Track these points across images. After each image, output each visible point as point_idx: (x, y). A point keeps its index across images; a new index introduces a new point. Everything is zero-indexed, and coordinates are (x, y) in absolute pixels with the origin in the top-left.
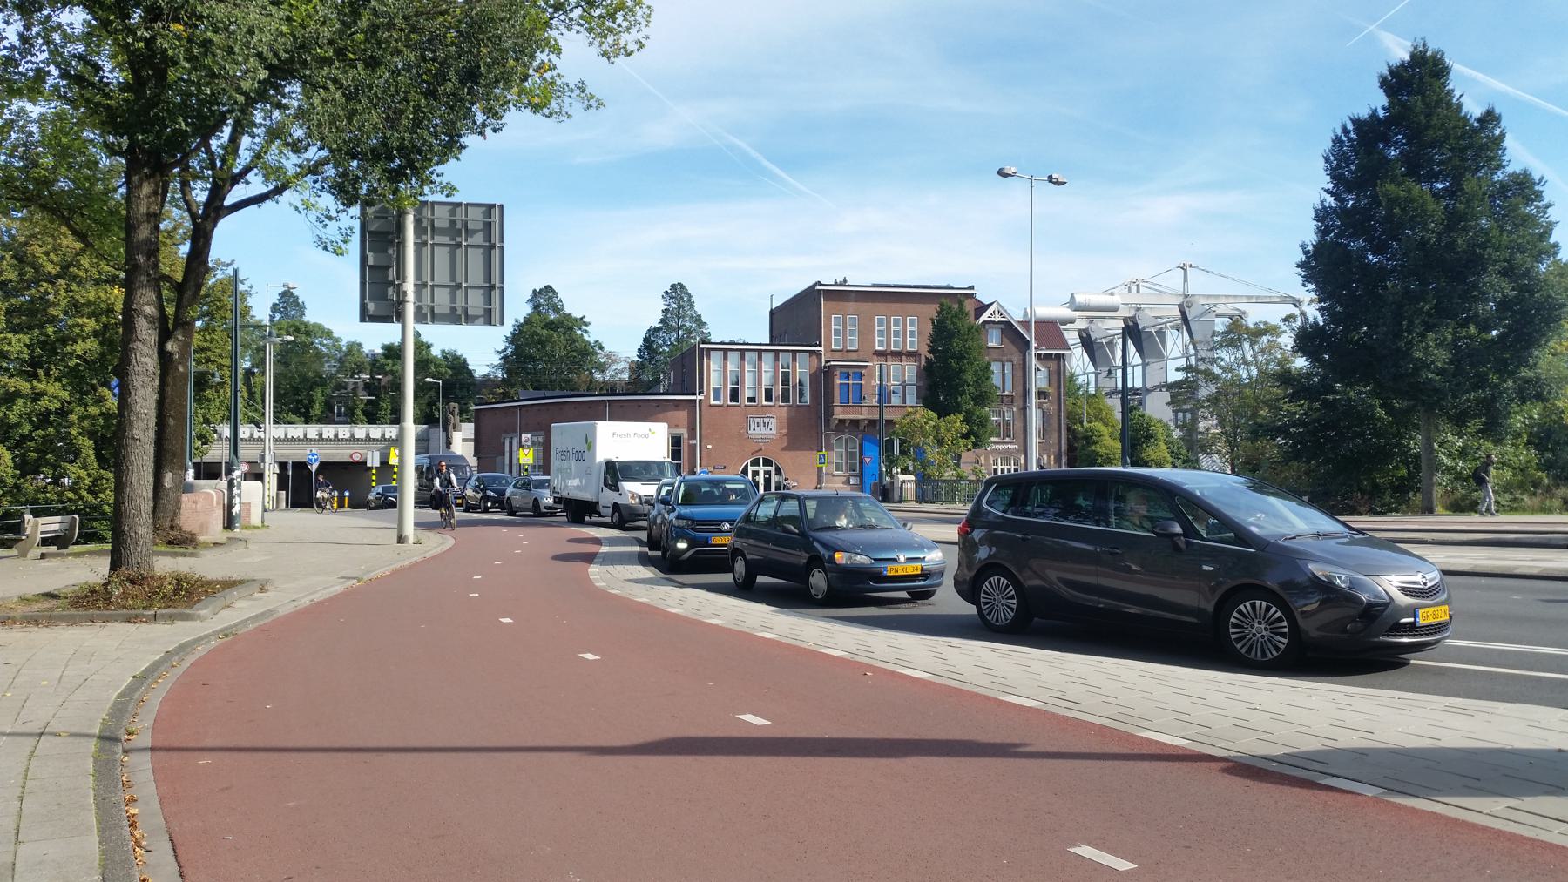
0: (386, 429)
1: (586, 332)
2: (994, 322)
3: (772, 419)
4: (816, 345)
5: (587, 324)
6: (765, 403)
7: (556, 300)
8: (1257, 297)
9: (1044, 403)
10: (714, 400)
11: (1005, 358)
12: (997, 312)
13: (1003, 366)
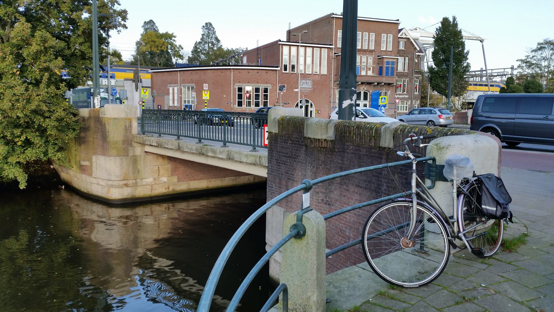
0: (103, 80)
1: (175, 41)
2: (402, 38)
3: (310, 81)
4: (330, 45)
5: (175, 37)
6: (284, 72)
7: (154, 27)
8: (468, 37)
9: (420, 76)
10: (284, 71)
11: (405, 55)
12: (404, 33)
13: (405, 59)
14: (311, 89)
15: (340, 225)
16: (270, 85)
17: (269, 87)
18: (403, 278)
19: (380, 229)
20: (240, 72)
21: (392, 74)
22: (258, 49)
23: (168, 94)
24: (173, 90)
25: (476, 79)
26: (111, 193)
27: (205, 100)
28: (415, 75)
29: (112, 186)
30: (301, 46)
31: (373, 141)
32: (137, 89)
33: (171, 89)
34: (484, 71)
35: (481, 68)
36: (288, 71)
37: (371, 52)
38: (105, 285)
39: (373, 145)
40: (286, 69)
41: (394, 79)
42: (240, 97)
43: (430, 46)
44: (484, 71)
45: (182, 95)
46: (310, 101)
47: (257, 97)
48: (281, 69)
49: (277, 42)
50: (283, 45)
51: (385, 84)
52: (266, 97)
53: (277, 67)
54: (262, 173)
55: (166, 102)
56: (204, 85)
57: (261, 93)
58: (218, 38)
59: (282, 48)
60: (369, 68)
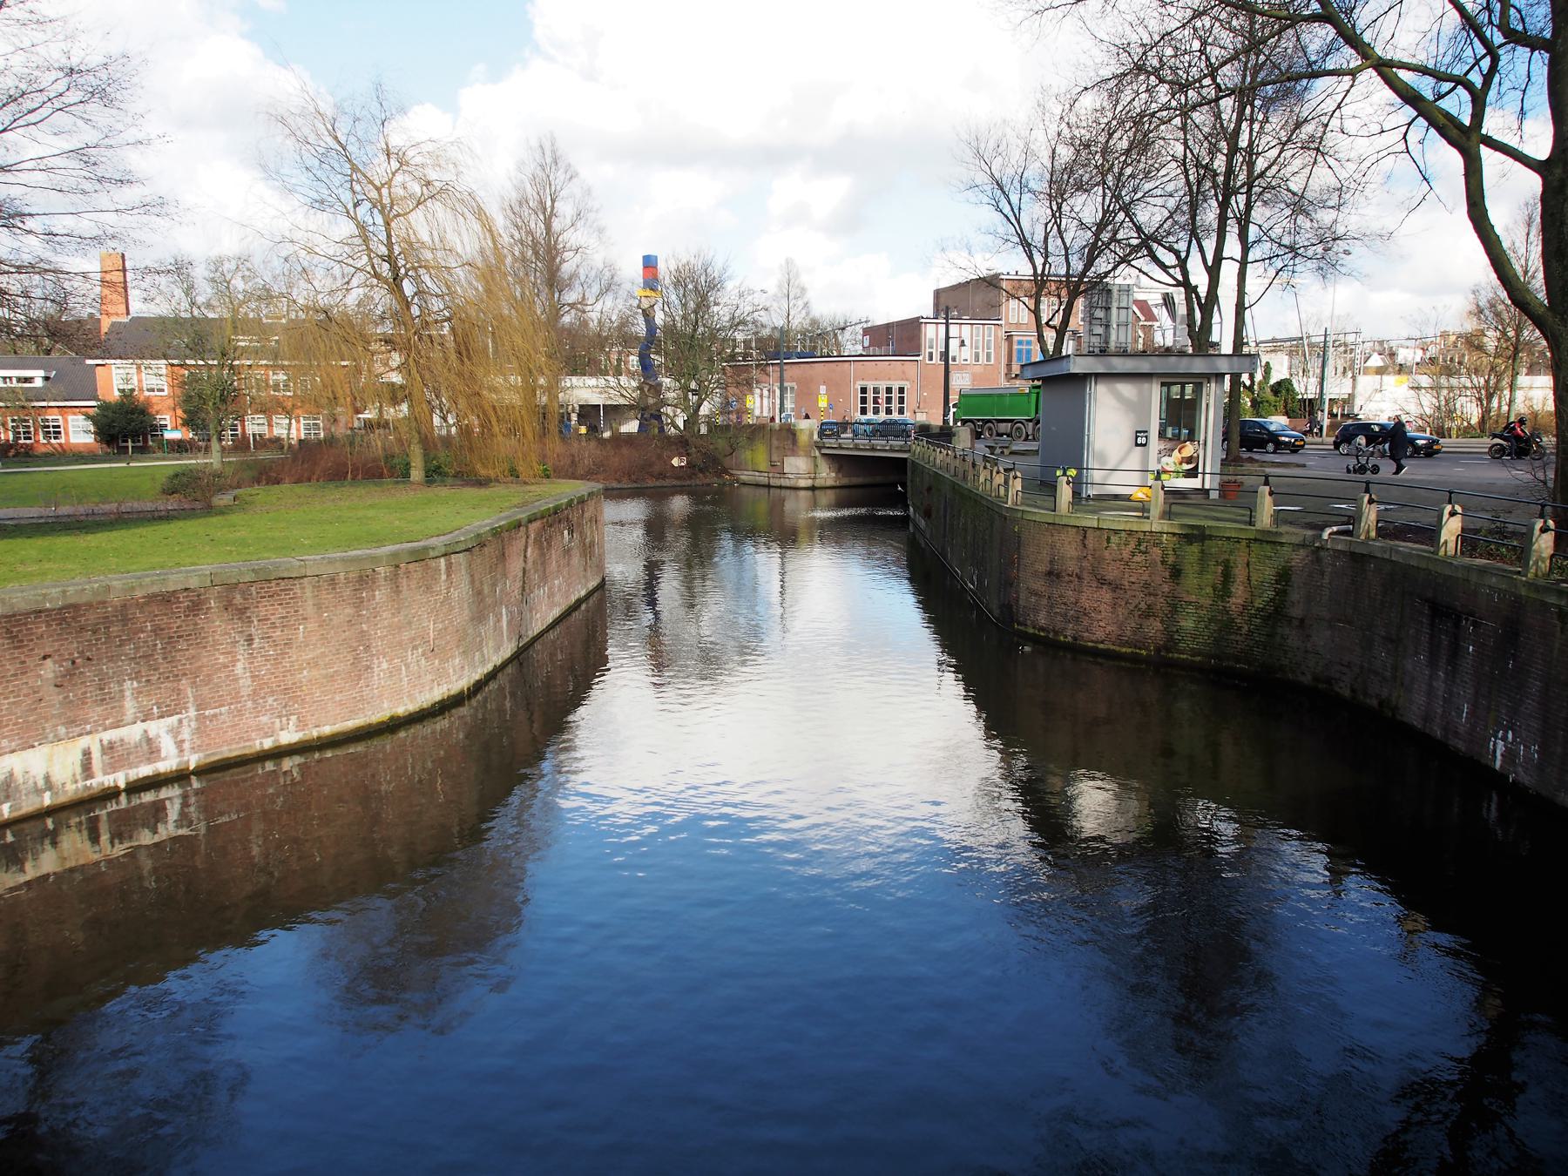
6: (928, 362)
16: (908, 383)
17: (907, 385)
18: (1184, 1001)
22: (888, 326)
29: (800, 478)
36: (933, 362)
38: (391, 882)
40: (931, 359)
48: (924, 358)
49: (918, 318)
52: (901, 400)
53: (918, 355)
57: (895, 395)
58: (880, 319)
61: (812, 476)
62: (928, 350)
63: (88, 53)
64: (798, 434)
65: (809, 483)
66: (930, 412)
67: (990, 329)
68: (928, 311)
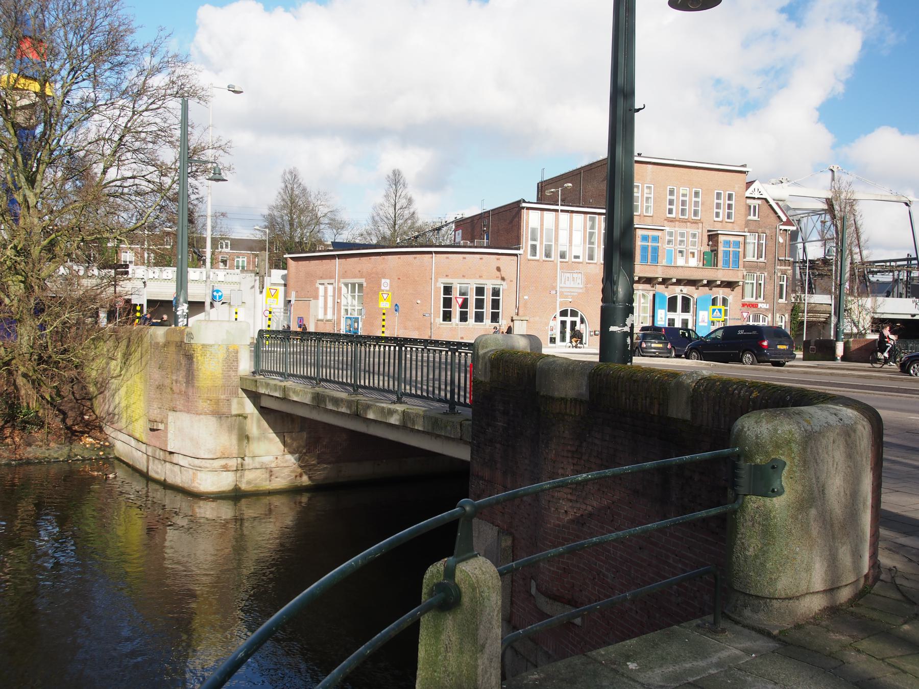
3: (580, 275)
6: (530, 257)
11: (760, 230)
12: (756, 190)
14: (580, 291)
15: (598, 562)
19: (668, 575)
20: (447, 258)
21: (736, 263)
23: (316, 297)
24: (325, 291)
25: (898, 275)
26: (199, 481)
27: (382, 309)
28: (778, 267)
30: (562, 211)
31: (656, 406)
32: (263, 288)
33: (321, 288)
34: (914, 259)
35: (908, 255)
36: (537, 257)
37: (696, 223)
39: (656, 413)
41: (740, 274)
42: (447, 303)
43: (808, 213)
44: (914, 259)
45: (341, 299)
46: (580, 313)
47: (480, 304)
49: (519, 202)
50: (528, 208)
51: (722, 282)
53: (518, 249)
54: (463, 453)
55: (312, 311)
56: (383, 281)
57: (488, 298)
59: (528, 214)
60: (691, 253)
61: (233, 463)
62: (530, 243)
63: (224, 211)
64: (198, 356)
65: (223, 482)
66: (531, 320)
67: (593, 220)
68: (531, 195)
